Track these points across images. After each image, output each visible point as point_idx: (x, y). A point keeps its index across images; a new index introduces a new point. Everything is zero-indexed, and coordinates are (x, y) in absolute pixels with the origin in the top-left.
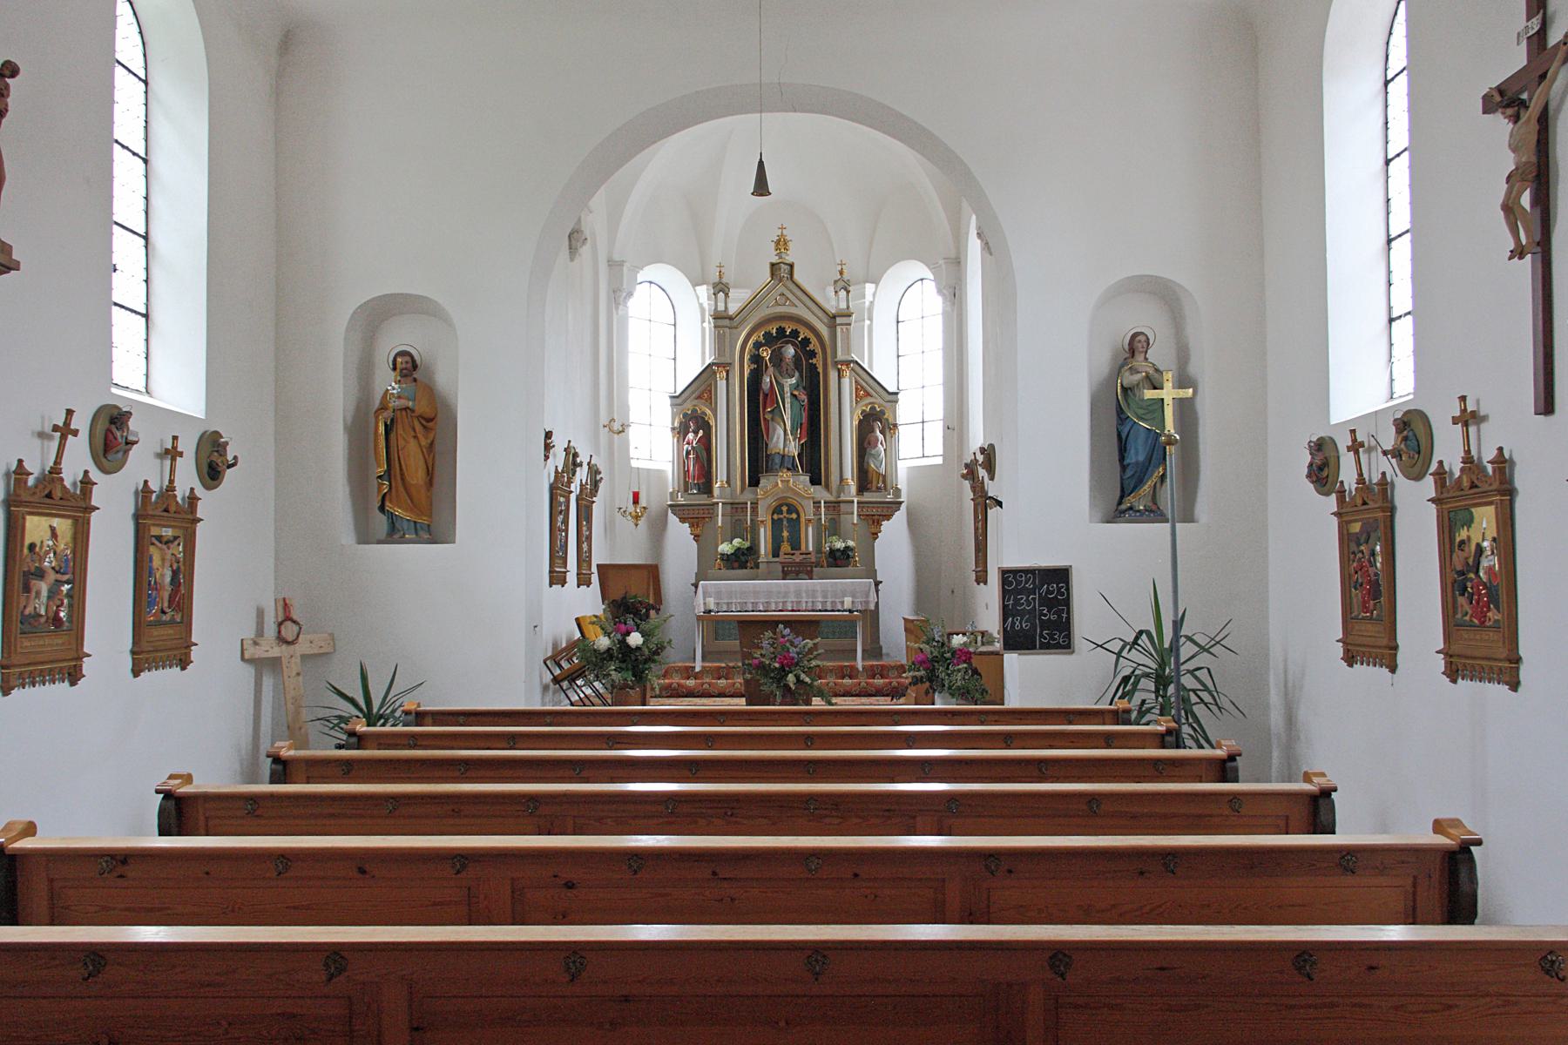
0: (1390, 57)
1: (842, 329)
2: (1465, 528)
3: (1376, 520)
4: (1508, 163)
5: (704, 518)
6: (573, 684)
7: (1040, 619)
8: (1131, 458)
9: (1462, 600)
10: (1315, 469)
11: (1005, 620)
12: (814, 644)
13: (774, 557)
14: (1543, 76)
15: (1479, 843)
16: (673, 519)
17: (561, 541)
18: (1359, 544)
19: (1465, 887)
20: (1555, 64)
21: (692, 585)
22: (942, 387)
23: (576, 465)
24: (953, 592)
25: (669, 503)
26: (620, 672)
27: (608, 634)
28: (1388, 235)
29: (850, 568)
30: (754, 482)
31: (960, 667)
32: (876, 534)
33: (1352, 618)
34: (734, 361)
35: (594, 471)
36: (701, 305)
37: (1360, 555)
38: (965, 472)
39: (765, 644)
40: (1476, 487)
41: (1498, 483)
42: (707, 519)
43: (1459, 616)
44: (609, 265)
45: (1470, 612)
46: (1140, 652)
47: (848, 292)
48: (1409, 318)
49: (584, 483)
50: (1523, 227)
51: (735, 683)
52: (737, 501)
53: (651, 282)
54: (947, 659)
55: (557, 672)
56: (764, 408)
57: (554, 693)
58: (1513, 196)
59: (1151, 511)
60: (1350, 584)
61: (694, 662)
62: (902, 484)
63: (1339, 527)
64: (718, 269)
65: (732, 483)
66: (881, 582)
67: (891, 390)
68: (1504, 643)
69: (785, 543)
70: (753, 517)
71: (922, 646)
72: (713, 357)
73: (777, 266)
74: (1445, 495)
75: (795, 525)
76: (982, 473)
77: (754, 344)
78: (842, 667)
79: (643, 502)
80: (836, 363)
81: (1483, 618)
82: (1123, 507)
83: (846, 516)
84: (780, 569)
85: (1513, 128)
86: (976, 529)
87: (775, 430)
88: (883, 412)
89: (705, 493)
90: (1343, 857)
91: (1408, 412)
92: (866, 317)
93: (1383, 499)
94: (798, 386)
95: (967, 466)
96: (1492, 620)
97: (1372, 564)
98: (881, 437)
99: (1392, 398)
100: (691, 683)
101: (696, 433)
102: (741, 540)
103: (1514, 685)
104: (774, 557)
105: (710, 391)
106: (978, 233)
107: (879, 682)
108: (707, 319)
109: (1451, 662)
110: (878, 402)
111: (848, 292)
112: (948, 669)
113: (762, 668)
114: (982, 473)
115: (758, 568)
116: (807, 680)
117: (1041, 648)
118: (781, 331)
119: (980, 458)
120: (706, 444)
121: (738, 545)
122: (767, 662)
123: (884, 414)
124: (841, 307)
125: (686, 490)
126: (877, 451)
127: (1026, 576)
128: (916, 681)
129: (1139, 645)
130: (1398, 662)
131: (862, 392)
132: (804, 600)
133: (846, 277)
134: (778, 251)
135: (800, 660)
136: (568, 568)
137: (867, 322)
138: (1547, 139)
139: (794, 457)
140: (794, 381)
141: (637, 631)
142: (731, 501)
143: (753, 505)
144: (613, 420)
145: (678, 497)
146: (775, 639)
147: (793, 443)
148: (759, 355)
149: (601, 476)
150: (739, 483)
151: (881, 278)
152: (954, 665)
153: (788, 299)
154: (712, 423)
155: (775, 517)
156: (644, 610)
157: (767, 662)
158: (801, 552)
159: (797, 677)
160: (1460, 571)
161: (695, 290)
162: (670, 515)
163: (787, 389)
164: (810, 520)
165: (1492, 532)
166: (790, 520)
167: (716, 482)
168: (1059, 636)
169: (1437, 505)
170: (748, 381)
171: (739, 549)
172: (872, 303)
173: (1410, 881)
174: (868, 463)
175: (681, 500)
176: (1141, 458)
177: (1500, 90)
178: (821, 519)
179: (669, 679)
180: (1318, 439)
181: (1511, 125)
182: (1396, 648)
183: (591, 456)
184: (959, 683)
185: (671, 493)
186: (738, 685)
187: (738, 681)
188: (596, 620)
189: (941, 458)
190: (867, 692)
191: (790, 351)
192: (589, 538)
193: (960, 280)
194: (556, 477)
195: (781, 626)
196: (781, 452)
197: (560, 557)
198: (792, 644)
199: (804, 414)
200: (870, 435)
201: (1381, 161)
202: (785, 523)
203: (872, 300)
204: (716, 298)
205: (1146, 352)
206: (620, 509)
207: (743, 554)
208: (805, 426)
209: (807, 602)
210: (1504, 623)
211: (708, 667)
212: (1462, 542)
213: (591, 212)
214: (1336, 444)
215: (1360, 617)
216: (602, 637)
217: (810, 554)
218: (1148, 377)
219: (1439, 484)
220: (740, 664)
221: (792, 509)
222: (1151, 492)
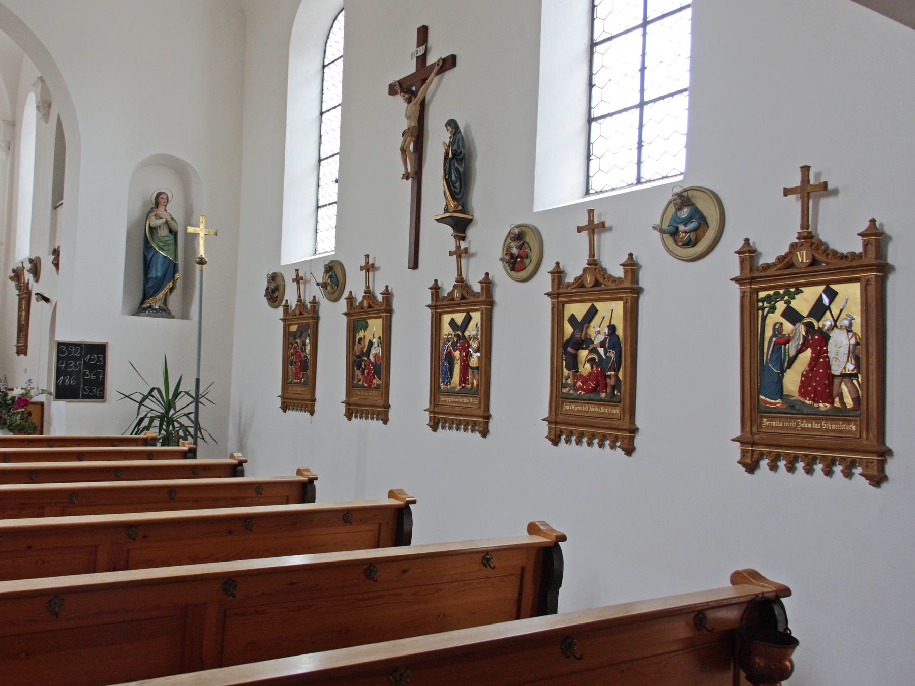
0: (327, 51)
2: (363, 330)
3: (308, 324)
4: (404, 125)
7: (84, 379)
8: (153, 274)
9: (358, 372)
10: (271, 291)
14: (424, 81)
15: (414, 502)
18: (295, 338)
19: (406, 528)
20: (433, 74)
28: (320, 157)
31: (19, 410)
33: (288, 383)
37: (296, 345)
38: (12, 275)
40: (371, 307)
41: (385, 306)
43: (355, 382)
45: (362, 379)
46: (153, 402)
48: (335, 205)
50: (410, 162)
54: (8, 405)
58: (406, 144)
59: (163, 310)
60: (288, 362)
63: (284, 327)
68: (382, 397)
74: (352, 311)
76: (28, 276)
81: (370, 382)
82: (145, 306)
85: (407, 107)
86: (20, 316)
90: (345, 515)
91: (332, 262)
93: (313, 312)
95: (14, 271)
96: (375, 384)
97: (303, 351)
99: (315, 253)
103: (386, 421)
109: (349, 409)
112: (9, 411)
114: (28, 276)
117: (82, 398)
119: (28, 266)
127: (75, 348)
129: (153, 396)
130: (315, 409)
138: (424, 115)
152: (14, 408)
160: (358, 356)
165: (379, 333)
168: (96, 391)
169: (347, 317)
173: (376, 527)
176: (159, 275)
177: (400, 83)
180: (273, 274)
181: (406, 104)
182: (314, 400)
184: (18, 422)
193: (15, 138)
201: (318, 113)
205: (166, 206)
210: (383, 385)
212: (360, 339)
214: (283, 278)
215: (293, 382)
218: (167, 222)
219: (349, 305)
222: (164, 298)
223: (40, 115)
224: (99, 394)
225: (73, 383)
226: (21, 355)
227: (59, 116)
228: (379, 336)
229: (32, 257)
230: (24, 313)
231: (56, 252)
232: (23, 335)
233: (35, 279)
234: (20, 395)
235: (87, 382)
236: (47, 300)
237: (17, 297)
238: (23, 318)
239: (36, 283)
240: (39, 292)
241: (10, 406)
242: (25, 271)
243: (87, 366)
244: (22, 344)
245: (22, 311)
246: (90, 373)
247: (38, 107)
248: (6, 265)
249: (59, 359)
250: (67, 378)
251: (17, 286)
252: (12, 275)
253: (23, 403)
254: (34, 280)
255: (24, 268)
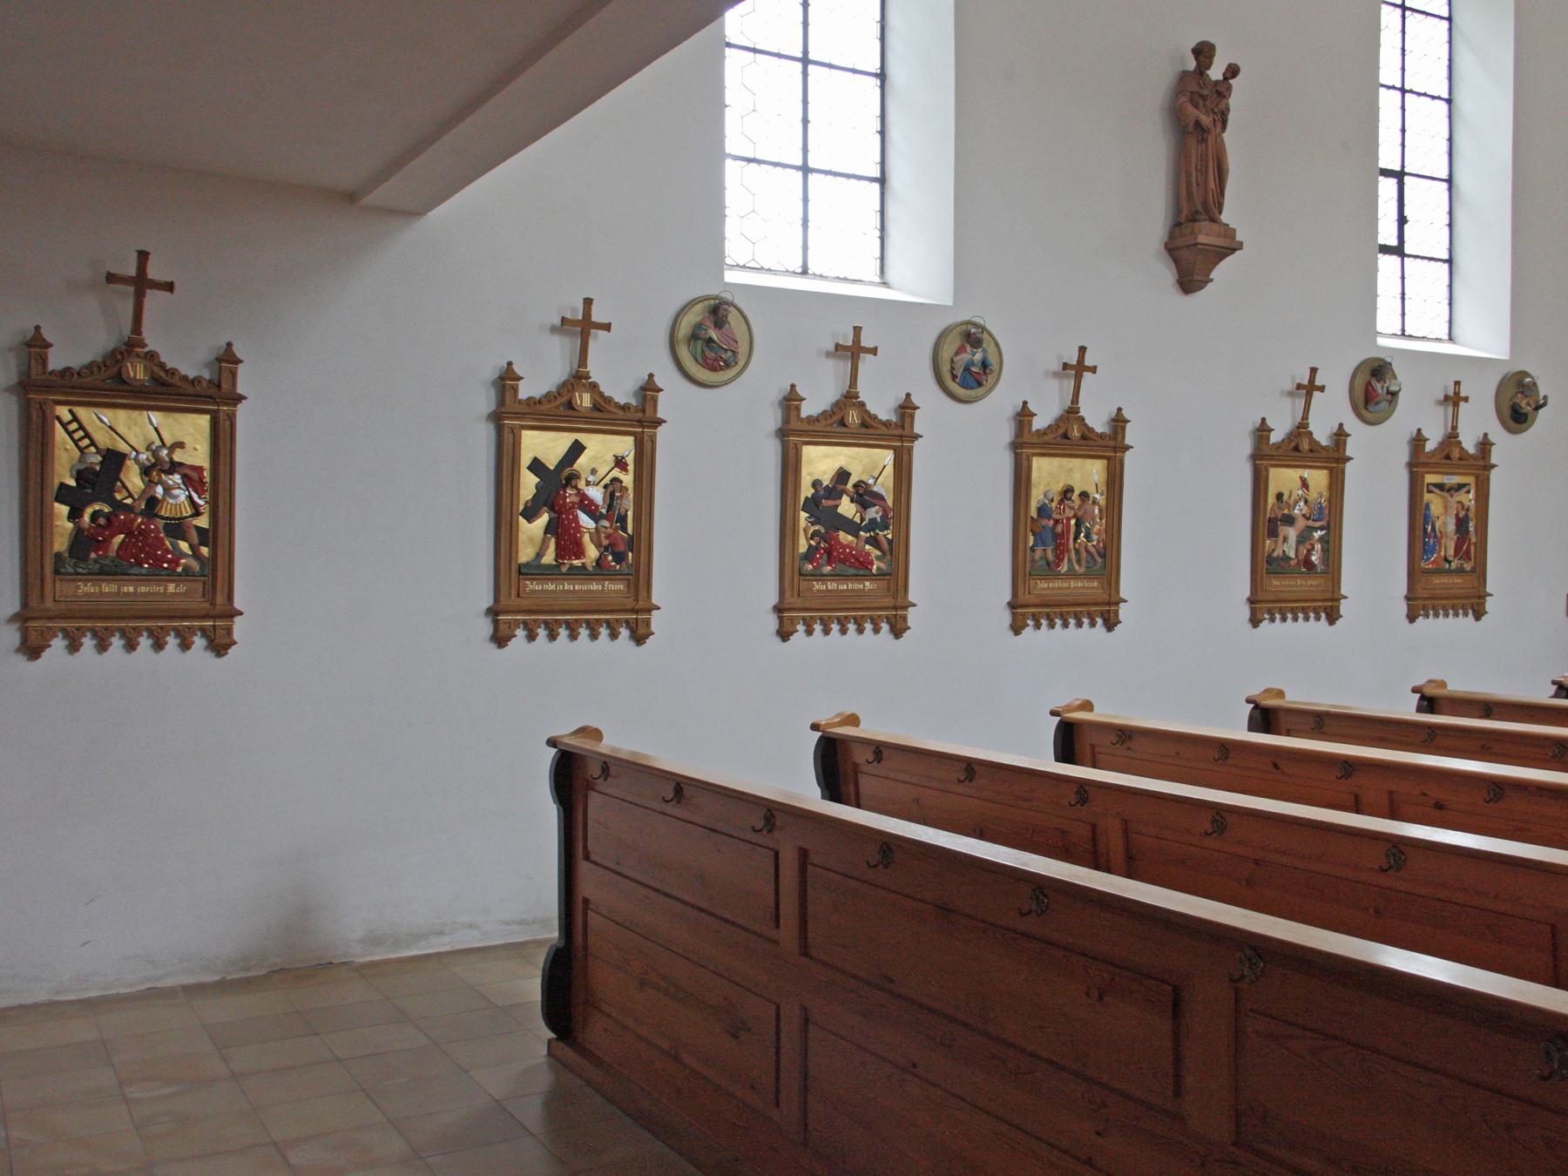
228: (850, 469)
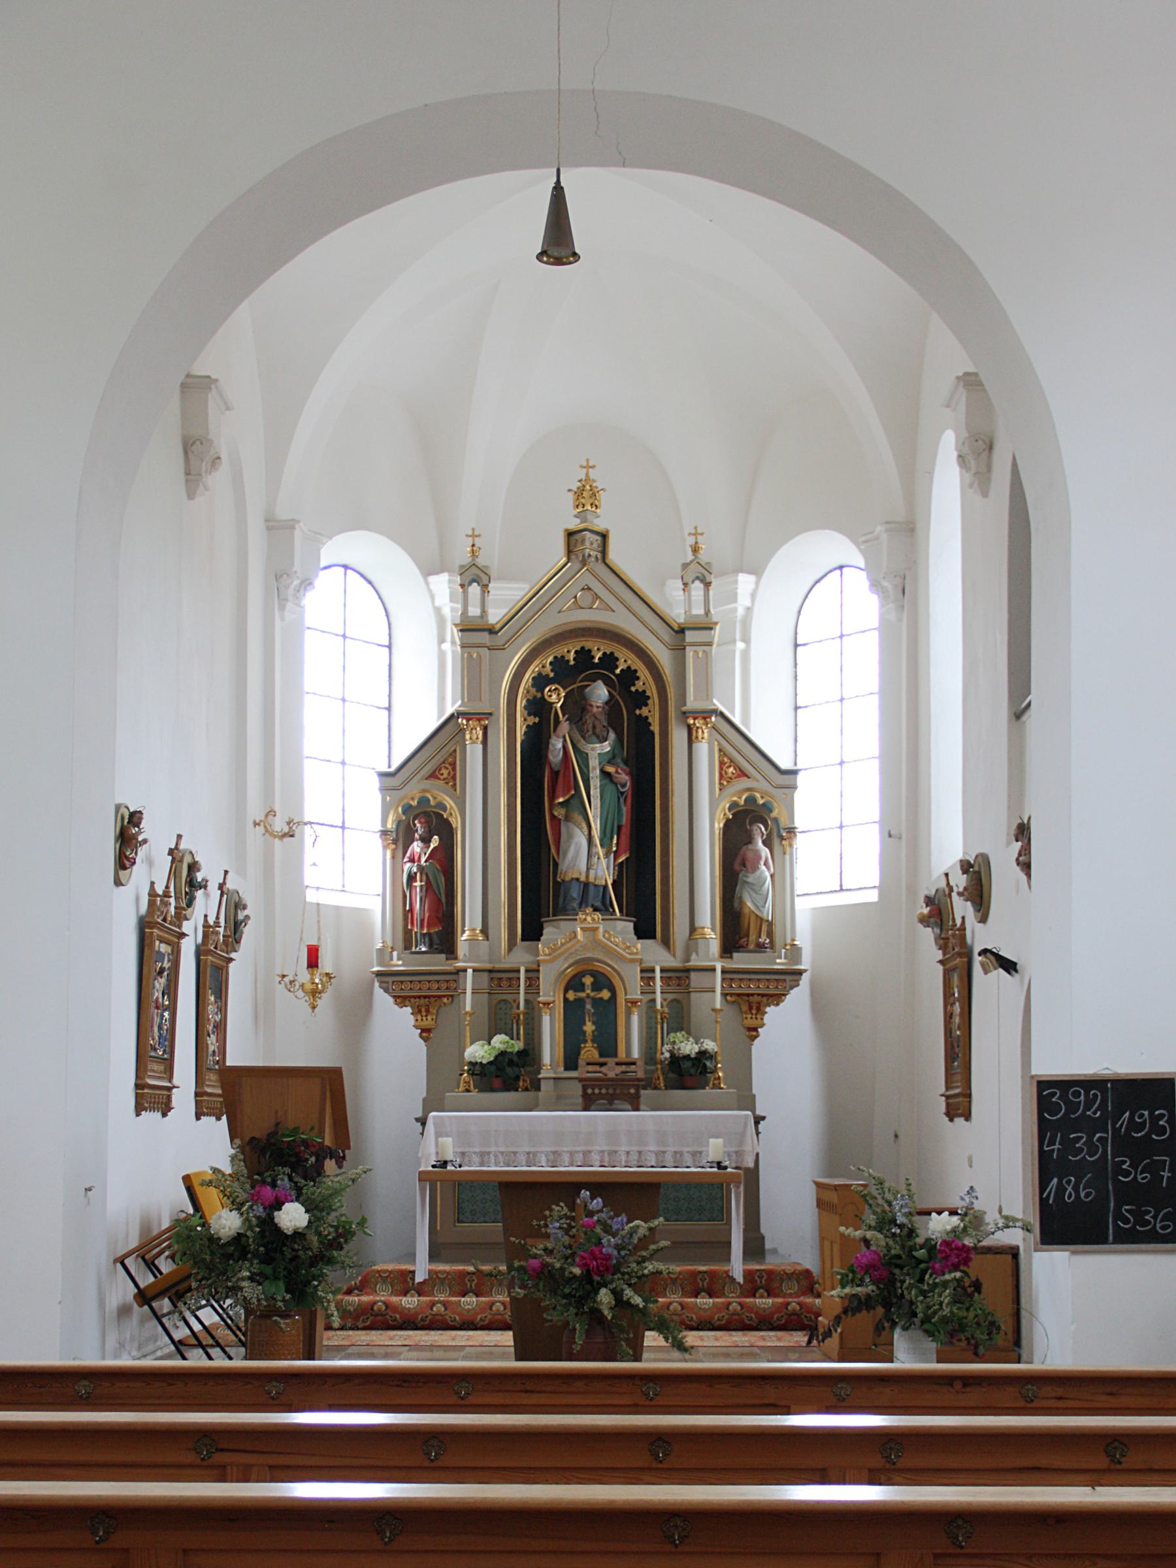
1: (696, 652)
5: (440, 997)
6: (180, 1304)
7: (1116, 1182)
11: (1043, 1184)
12: (650, 1229)
13: (566, 1069)
16: (382, 1000)
17: (160, 1028)
21: (417, 1120)
22: (876, 762)
23: (194, 885)
24: (896, 1136)
25: (376, 969)
26: (260, 1284)
27: (237, 1206)
29: (708, 1090)
30: (532, 932)
31: (947, 1277)
32: (755, 1030)
34: (499, 708)
35: (234, 906)
36: (438, 611)
38: (926, 911)
39: (554, 1227)
42: (445, 1000)
44: (269, 529)
47: (707, 585)
49: (211, 921)
51: (493, 1304)
52: (498, 966)
53: (346, 567)
54: (919, 1261)
55: (146, 1280)
56: (553, 797)
57: (142, 1322)
61: (413, 1262)
62: (803, 940)
64: (470, 541)
65: (490, 932)
66: (763, 1118)
67: (785, 764)
69: (589, 1044)
70: (530, 997)
71: (869, 1234)
72: (459, 702)
73: (577, 537)
75: (607, 1012)
76: (962, 909)
77: (534, 679)
78: (694, 1275)
79: (326, 963)
80: (685, 715)
83: (698, 995)
84: (580, 1092)
86: (948, 1017)
87: (570, 836)
88: (767, 807)
89: (441, 952)
92: (738, 636)
94: (614, 757)
95: (929, 901)
98: (765, 852)
100: (410, 1302)
101: (426, 840)
102: (507, 1038)
104: (566, 1069)
105: (453, 765)
106: (960, 456)
107: (764, 1302)
108: (449, 638)
110: (760, 787)
111: (707, 585)
112: (921, 1280)
113: (547, 1277)
114: (962, 909)
115: (538, 1089)
116: (638, 1300)
118: (584, 655)
119: (960, 881)
120: (445, 860)
121: (502, 1047)
122: (558, 1265)
123: (771, 811)
124: (695, 612)
125: (407, 946)
126: (759, 877)
128: (854, 1306)
131: (731, 769)
132: (624, 1148)
133: (703, 556)
134: (580, 509)
135: (622, 1261)
136: (176, 1081)
137: (740, 645)
139: (605, 887)
140: (606, 747)
141: (297, 1200)
142: (488, 966)
143: (530, 975)
144: (271, 813)
145: (392, 959)
146: (573, 1219)
147: (604, 862)
148: (543, 697)
149: (246, 912)
150: (504, 935)
151: (765, 566)
153: (597, 597)
154: (456, 822)
155: (571, 996)
156: (313, 1159)
157: (558, 1265)
158: (616, 1060)
159: (617, 1294)
161: (427, 584)
162: (378, 992)
163: (594, 762)
164: (634, 1003)
166: (597, 1002)
167: (463, 932)
168: (1155, 1217)
170: (521, 744)
171: (503, 1054)
172: (749, 610)
174: (741, 902)
175: (398, 964)
178: (654, 1001)
179: (368, 1294)
183: (226, 872)
184: (946, 1311)
185: (381, 952)
186: (499, 1307)
187: (500, 1299)
188: (217, 1179)
189: (876, 892)
190: (742, 1321)
191: (600, 693)
192: (221, 1028)
194: (151, 903)
195: (585, 1194)
196: (583, 878)
197: (161, 1060)
198: (607, 1229)
199: (624, 809)
200: (744, 848)
202: (588, 1006)
203: (749, 604)
204: (465, 594)
206: (284, 976)
207: (511, 1063)
208: (626, 831)
209: (628, 1153)
211: (445, 1272)
213: (228, 409)
216: (225, 1213)
217: (634, 1064)
220: (503, 1268)
221: (602, 981)
223: (968, 477)
224: (1163, 1228)
225: (1087, 1195)
226: (956, 1120)
227: (1014, 459)
228: (978, 1201)
229: (968, 858)
230: (957, 1008)
231: (1023, 832)
232: (958, 1066)
233: (979, 915)
234: (948, 1233)
235: (1125, 1193)
236: (1009, 966)
237: (940, 968)
238: (957, 1020)
239: (981, 925)
240: (989, 948)
241: (923, 1266)
242: (954, 895)
243: (1124, 1144)
244: (957, 1091)
245: (953, 1004)
246: (1134, 1165)
247: (961, 458)
248: (912, 889)
249: (1044, 1127)
250: (1069, 1182)
251: (938, 939)
252: (926, 911)
253: (958, 1256)
254: (976, 918)
255: (951, 889)
